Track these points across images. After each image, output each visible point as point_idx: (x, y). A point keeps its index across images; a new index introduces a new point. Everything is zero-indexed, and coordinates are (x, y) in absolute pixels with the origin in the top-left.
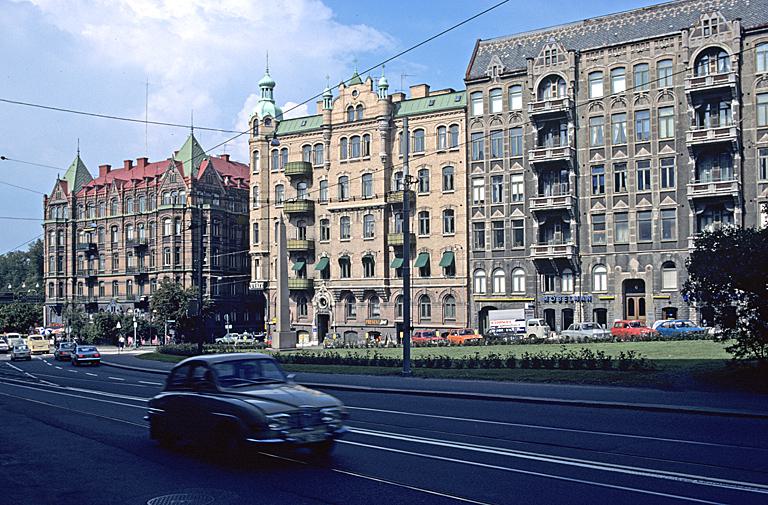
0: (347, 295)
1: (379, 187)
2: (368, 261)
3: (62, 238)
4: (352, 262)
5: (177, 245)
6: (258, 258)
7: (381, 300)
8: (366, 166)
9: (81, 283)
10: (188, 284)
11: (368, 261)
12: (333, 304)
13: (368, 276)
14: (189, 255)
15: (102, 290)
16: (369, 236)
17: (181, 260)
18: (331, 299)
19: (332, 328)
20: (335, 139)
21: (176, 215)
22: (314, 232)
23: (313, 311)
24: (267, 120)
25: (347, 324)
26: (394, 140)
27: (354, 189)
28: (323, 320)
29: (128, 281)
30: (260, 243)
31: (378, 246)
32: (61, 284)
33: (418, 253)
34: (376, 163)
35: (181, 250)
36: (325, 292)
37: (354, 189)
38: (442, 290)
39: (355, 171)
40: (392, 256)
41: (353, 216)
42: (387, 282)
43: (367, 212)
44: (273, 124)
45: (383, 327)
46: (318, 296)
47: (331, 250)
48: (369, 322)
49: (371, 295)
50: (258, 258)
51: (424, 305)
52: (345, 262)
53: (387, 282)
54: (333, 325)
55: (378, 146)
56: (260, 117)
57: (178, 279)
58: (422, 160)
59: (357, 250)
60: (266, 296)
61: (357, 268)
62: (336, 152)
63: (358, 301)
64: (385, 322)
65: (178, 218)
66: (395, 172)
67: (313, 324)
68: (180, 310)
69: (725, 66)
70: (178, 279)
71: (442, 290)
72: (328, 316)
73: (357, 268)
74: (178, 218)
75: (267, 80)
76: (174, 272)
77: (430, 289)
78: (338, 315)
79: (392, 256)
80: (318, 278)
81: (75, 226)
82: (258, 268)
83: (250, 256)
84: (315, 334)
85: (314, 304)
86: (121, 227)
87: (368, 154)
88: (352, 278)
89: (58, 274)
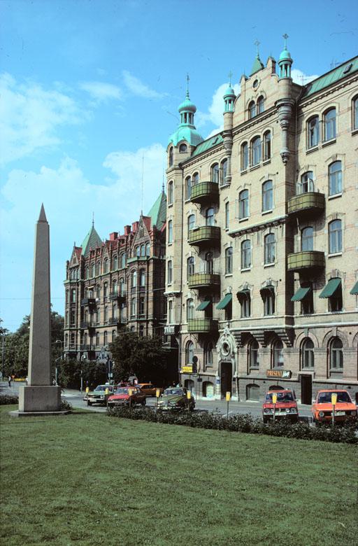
0: (246, 338)
1: (279, 194)
2: (268, 294)
3: (74, 296)
4: (252, 297)
5: (142, 295)
6: (171, 299)
7: (285, 346)
8: (264, 172)
9: (86, 334)
10: (150, 332)
11: (268, 294)
12: (236, 350)
13: (268, 313)
14: (151, 305)
15: (98, 339)
16: (269, 260)
17: (145, 310)
18: (232, 342)
19: (234, 379)
20: (237, 148)
21: (140, 267)
22: (219, 264)
23: (218, 356)
24: (182, 146)
25: (250, 376)
26: (299, 132)
27: (255, 203)
28: (226, 369)
29: (113, 331)
30: (172, 282)
31: (278, 274)
32: (73, 335)
33: (328, 278)
34: (277, 169)
35: (145, 300)
36: (227, 337)
37: (255, 203)
38: (327, 330)
39: (253, 181)
40: (297, 285)
41: (253, 237)
42: (290, 320)
43: (267, 231)
44: (189, 150)
45: (286, 380)
46: (221, 341)
47: (231, 285)
48: (271, 373)
49: (272, 337)
50: (171, 299)
51: (335, 352)
52: (244, 297)
53: (290, 320)
54: (235, 376)
55: (279, 143)
56: (175, 144)
57: (142, 327)
58: (331, 151)
59: (256, 279)
60: (178, 341)
61: (257, 303)
62: (236, 161)
63: (260, 346)
64: (288, 374)
65: (143, 269)
66: (301, 173)
67: (216, 374)
68: (132, 356)
69: (274, 443)
70: (142, 327)
71: (327, 330)
72: (231, 364)
73: (257, 303)
74: (143, 269)
75: (187, 103)
76: (137, 321)
77: (342, 329)
78: (240, 364)
79: (297, 285)
80: (223, 319)
81: (83, 284)
82: (172, 310)
83: (165, 298)
84: (218, 386)
85: (218, 350)
86: (109, 283)
87: (269, 158)
88: (252, 317)
89: (71, 326)
